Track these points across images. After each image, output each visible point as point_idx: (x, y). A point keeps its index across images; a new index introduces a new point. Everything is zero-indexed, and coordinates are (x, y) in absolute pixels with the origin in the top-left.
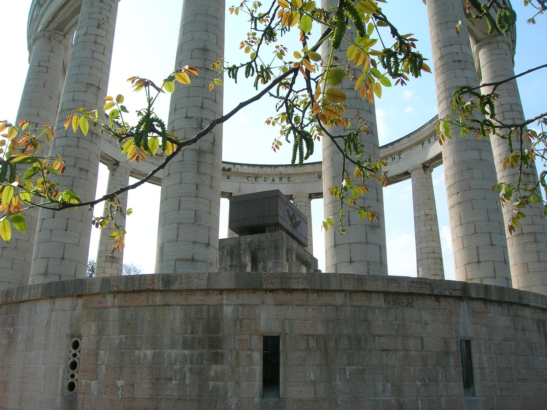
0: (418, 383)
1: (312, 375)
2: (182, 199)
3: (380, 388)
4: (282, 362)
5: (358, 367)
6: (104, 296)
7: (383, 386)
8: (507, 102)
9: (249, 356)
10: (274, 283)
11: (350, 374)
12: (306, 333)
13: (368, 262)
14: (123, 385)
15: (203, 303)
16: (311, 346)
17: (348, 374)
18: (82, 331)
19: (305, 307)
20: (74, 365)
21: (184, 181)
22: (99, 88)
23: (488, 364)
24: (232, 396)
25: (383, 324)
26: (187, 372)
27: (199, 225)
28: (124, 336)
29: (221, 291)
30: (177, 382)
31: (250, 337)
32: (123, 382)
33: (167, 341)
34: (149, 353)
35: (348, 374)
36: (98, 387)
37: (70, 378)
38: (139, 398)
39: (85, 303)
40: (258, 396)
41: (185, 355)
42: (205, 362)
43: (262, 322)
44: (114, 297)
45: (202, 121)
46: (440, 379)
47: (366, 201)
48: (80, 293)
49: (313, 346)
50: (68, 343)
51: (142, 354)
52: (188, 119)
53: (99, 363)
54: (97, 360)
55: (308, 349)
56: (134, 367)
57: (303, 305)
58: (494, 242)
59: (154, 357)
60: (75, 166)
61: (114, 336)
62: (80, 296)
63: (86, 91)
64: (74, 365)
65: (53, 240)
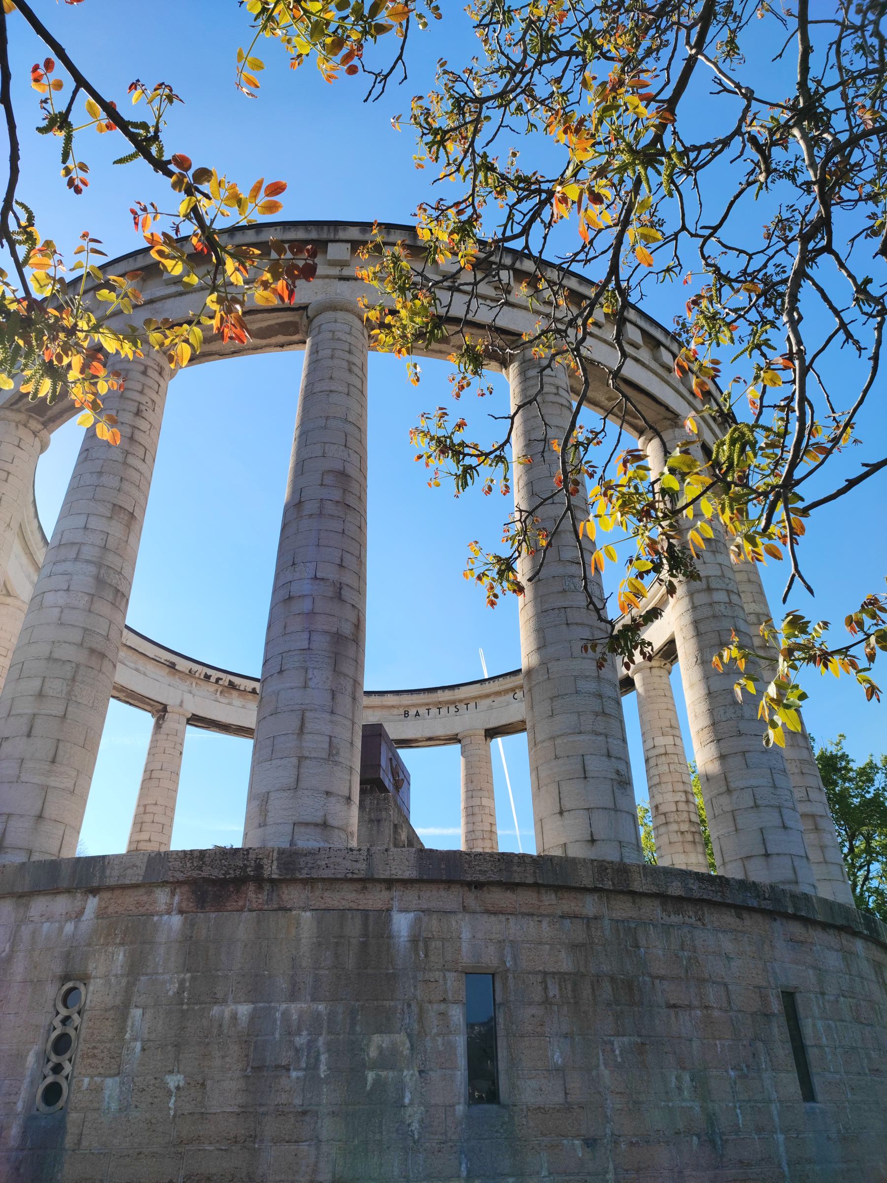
0: (732, 1073)
1: (558, 1054)
2: (307, 714)
3: (673, 1082)
4: (502, 1027)
5: (632, 1039)
6: (150, 893)
7: (676, 1078)
8: (752, 611)
9: (443, 1015)
10: (485, 871)
11: (621, 1054)
12: (541, 968)
13: (620, 842)
14: (181, 1084)
15: (354, 906)
16: (551, 994)
17: (617, 1052)
18: (91, 966)
19: (536, 918)
21: (311, 684)
22: (132, 514)
23: (827, 1039)
24: (411, 1104)
25: (664, 955)
26: (322, 1050)
27: (337, 763)
28: (188, 975)
29: (390, 883)
30: (301, 1074)
31: (444, 976)
32: (180, 1077)
33: (283, 984)
34: (244, 1010)
35: (617, 1052)
36: (121, 1091)
37: (51, 1073)
38: (215, 1114)
39: (103, 905)
40: (462, 1100)
41: (319, 1014)
42: (358, 1028)
43: (465, 947)
44: (173, 894)
45: (341, 589)
46: (764, 1066)
47: (609, 740)
48: (95, 884)
49: (555, 996)
50: (52, 992)
51: (227, 1014)
52: (317, 582)
53: (127, 1036)
54: (122, 1030)
55: (547, 1002)
56: (208, 1044)
57: (532, 915)
58: (789, 823)
59: (252, 1018)
60: (82, 644)
61: (167, 977)
62: (94, 891)
63: (111, 518)
64: (62, 1044)
65: (23, 778)
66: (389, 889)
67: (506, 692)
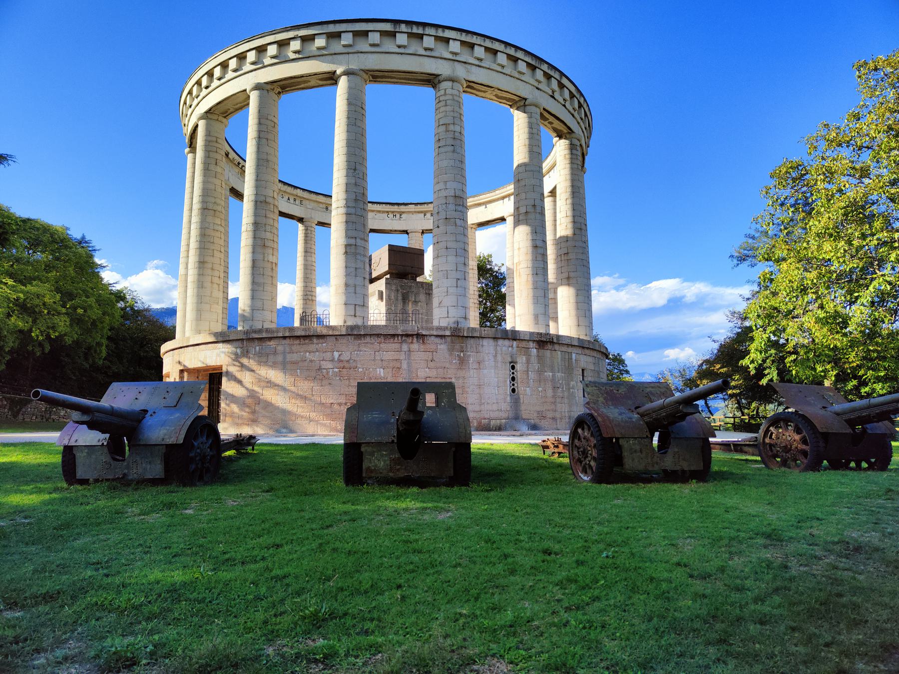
20: (513, 379)
34: (551, 374)
50: (508, 366)
62: (515, 340)
64: (513, 379)
66: (378, 337)
67: (383, 212)
